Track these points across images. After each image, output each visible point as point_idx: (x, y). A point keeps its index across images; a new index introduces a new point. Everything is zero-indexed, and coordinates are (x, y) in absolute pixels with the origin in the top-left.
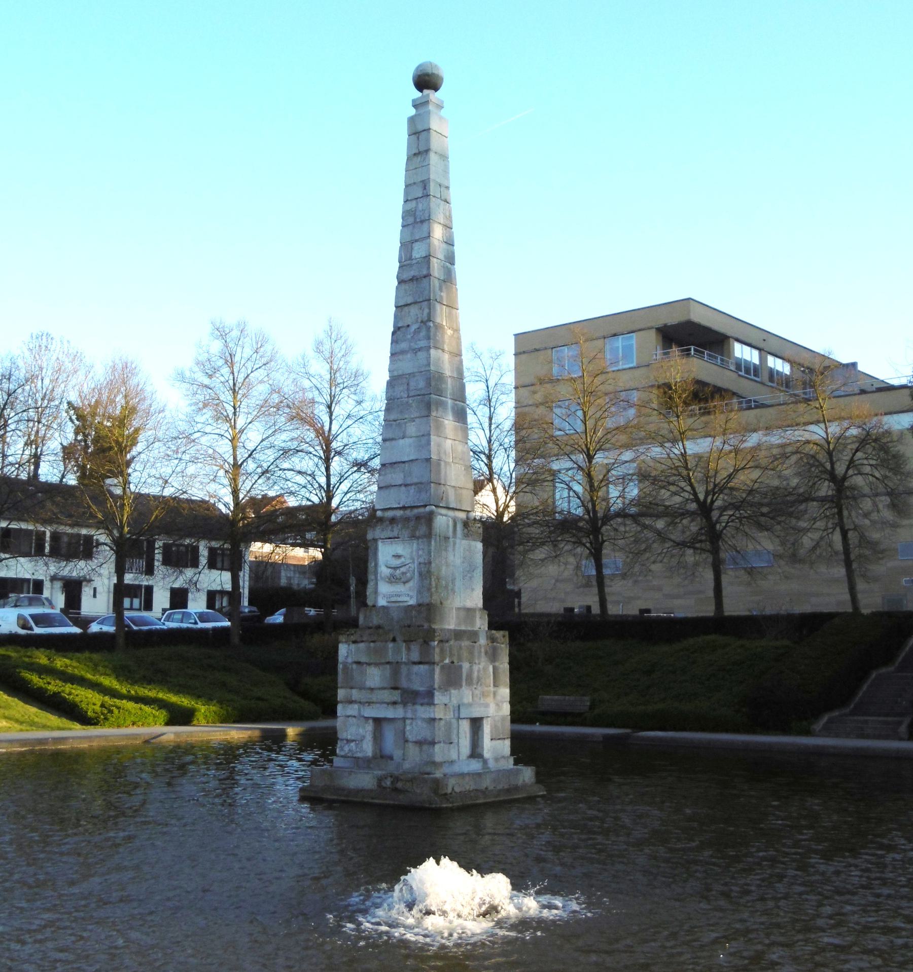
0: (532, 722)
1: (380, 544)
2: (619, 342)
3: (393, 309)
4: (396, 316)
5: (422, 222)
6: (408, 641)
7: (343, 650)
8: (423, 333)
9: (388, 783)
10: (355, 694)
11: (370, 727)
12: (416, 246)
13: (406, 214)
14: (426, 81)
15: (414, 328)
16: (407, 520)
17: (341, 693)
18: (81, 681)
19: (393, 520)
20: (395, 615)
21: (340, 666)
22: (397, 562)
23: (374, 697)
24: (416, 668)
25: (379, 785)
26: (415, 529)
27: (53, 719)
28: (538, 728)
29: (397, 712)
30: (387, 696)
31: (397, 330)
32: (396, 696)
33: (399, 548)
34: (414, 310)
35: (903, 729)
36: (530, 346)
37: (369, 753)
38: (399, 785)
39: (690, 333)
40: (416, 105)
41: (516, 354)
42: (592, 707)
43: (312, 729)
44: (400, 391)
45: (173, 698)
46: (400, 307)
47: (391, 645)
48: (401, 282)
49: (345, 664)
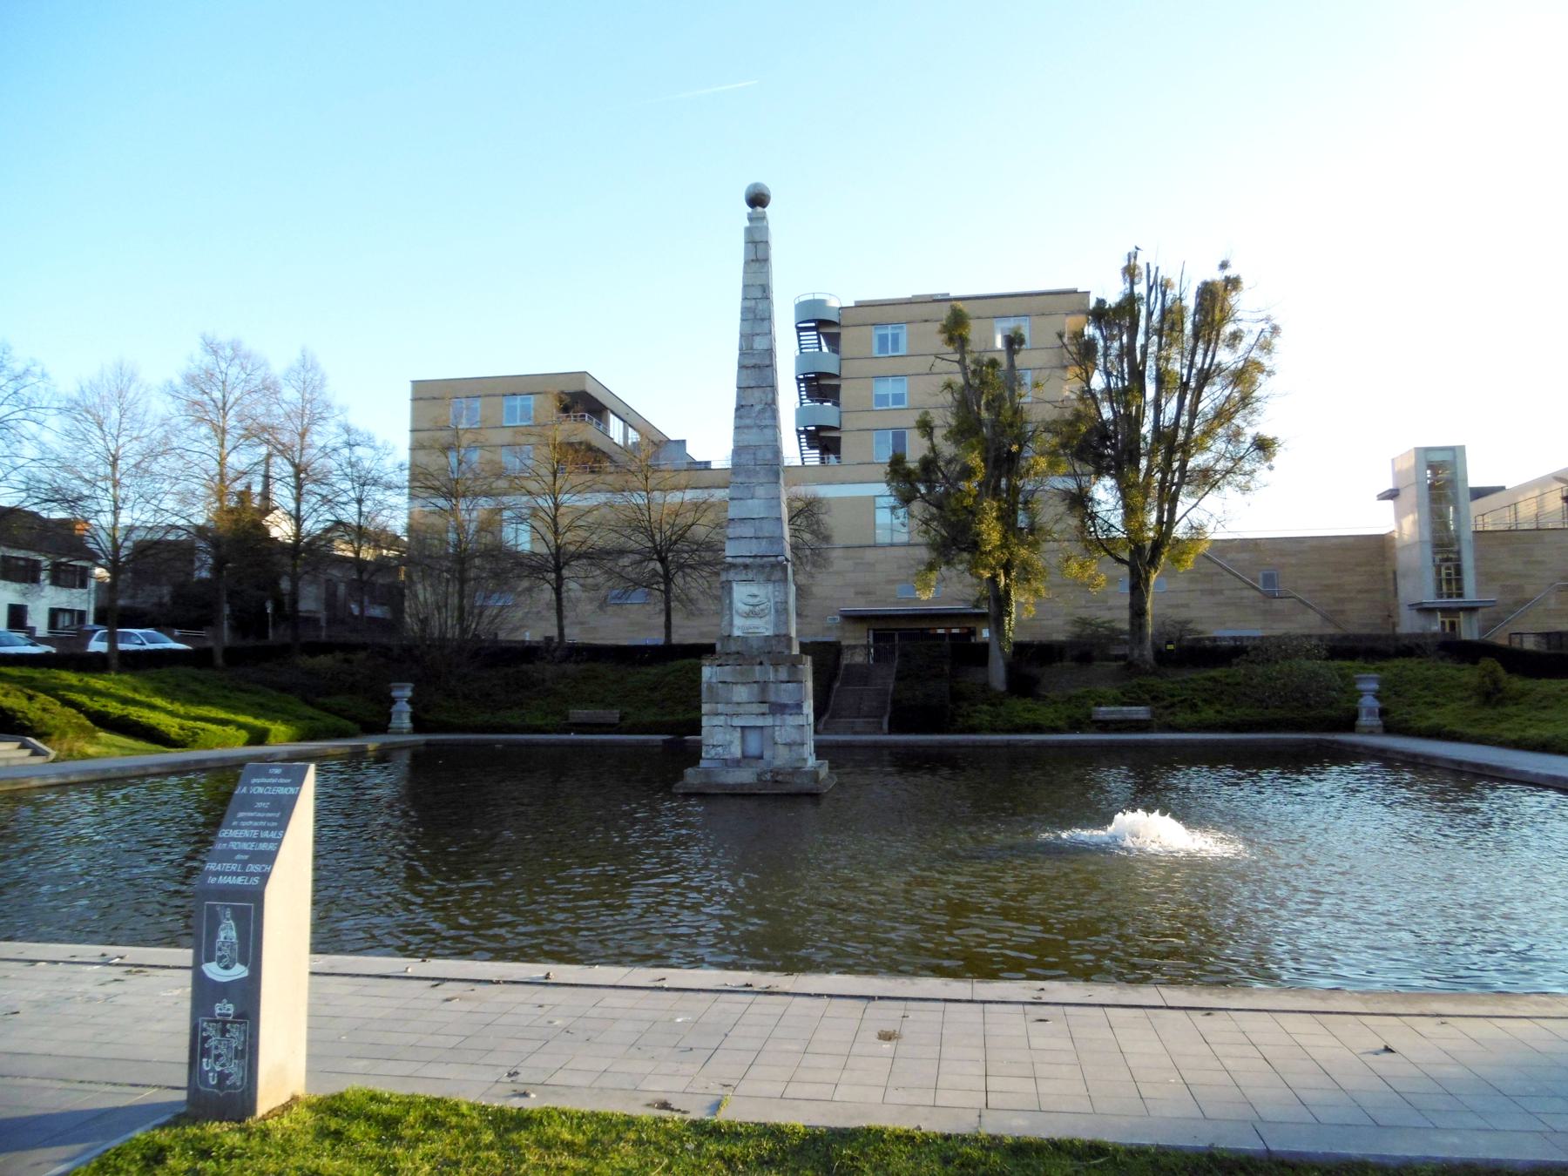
0: (568, 732)
1: (734, 585)
2: (518, 401)
3: (734, 391)
4: (738, 396)
5: (763, 320)
6: (776, 665)
7: (707, 672)
8: (768, 414)
9: (768, 777)
10: (721, 708)
11: (738, 734)
12: (757, 339)
13: (745, 310)
14: (757, 199)
15: (758, 407)
16: (763, 566)
17: (705, 708)
18: (153, 707)
19: (746, 566)
20: (755, 644)
21: (704, 686)
22: (755, 601)
23: (741, 710)
24: (784, 686)
25: (759, 780)
26: (771, 574)
27: (141, 745)
28: (572, 736)
29: (769, 721)
30: (756, 708)
31: (739, 408)
32: (765, 708)
33: (754, 589)
34: (757, 393)
35: (885, 726)
36: (427, 395)
37: (738, 754)
38: (780, 778)
39: (582, 402)
40: (751, 219)
41: (414, 400)
42: (622, 719)
43: (384, 744)
44: (746, 458)
45: (249, 720)
46: (741, 388)
47: (757, 668)
48: (742, 367)
49: (710, 685)
